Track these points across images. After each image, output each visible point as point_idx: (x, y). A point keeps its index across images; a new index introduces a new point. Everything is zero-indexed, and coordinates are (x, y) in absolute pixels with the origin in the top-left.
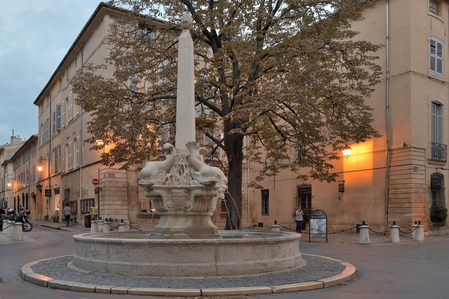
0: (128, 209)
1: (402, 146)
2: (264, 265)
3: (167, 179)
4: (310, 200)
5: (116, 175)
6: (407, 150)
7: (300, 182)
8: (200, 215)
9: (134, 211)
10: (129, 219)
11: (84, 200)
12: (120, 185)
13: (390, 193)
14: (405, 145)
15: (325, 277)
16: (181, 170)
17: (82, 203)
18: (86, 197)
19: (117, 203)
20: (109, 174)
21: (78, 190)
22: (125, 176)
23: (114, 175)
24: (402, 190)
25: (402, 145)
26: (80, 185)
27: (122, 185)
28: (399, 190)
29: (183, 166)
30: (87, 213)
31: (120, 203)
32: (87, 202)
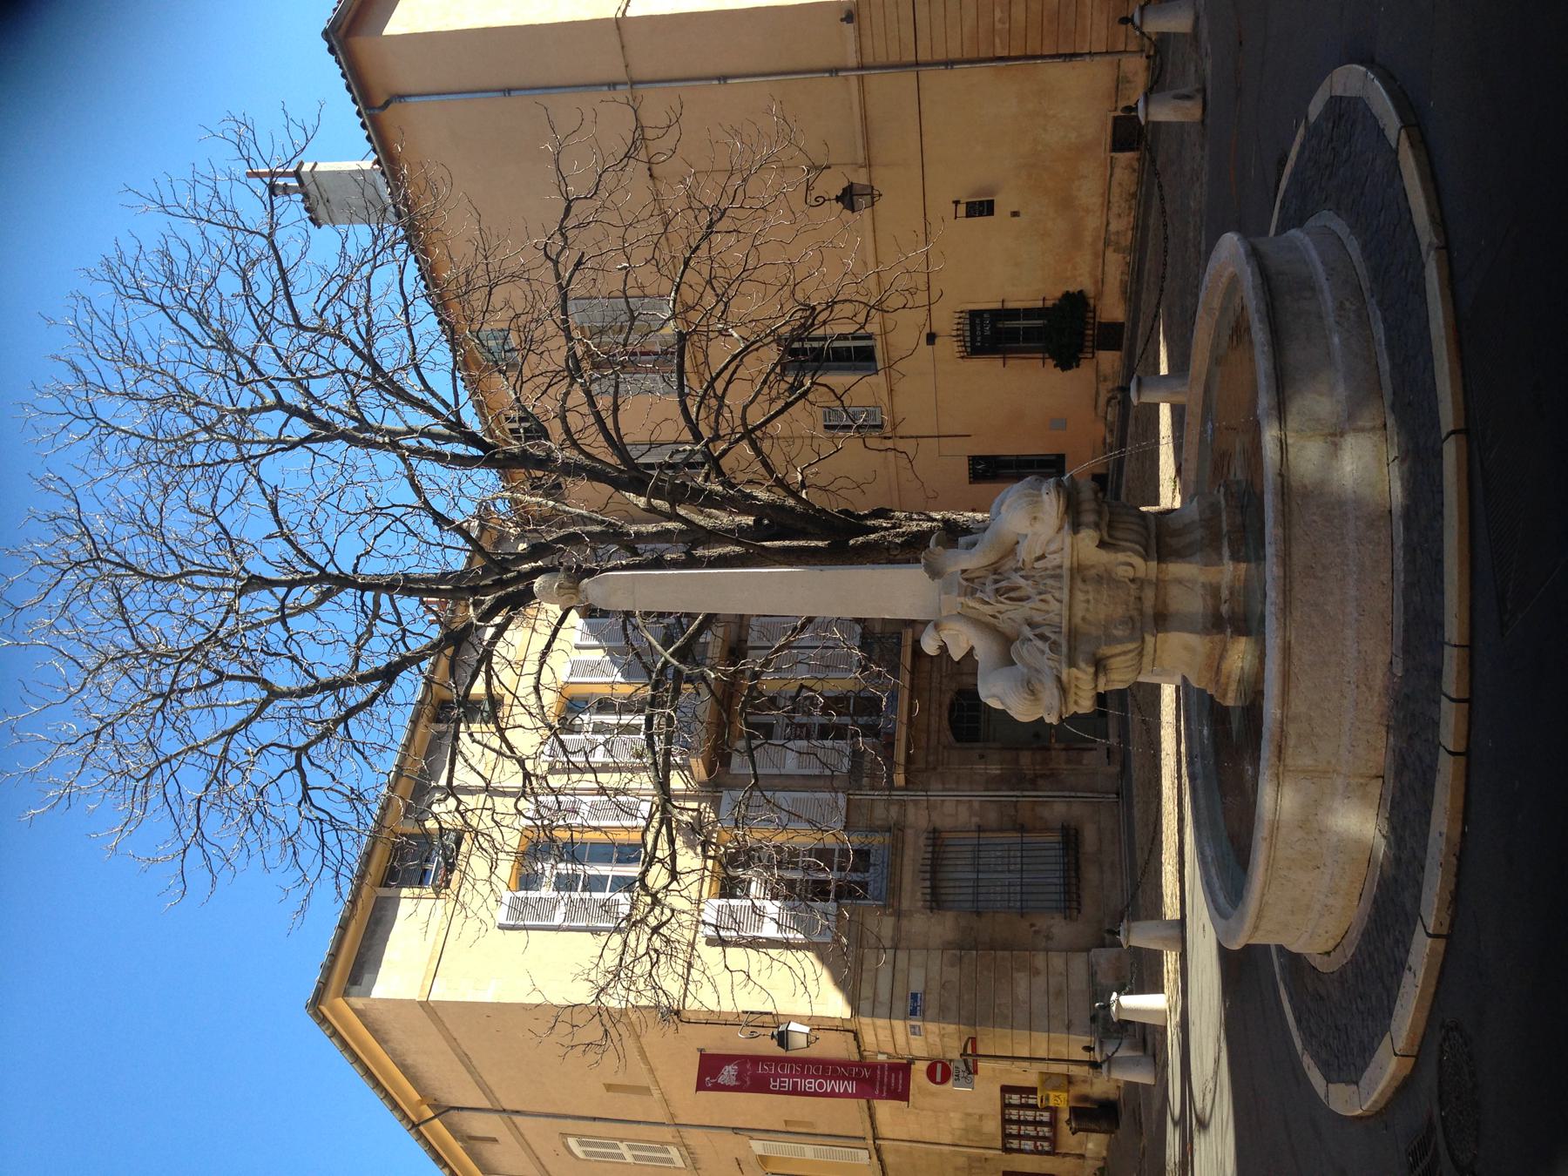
0: (1047, 950)
1: (851, 26)
2: (1341, 307)
3: (1042, 637)
4: (1014, 314)
5: (917, 986)
6: (864, 12)
7: (948, 347)
8: (1158, 537)
9: (1054, 930)
10: (1088, 950)
11: (1006, 1136)
12: (953, 974)
13: (1005, 53)
14: (849, 18)
15: (1381, 133)
16: (1012, 595)
17: (1015, 1144)
18: (993, 1126)
19: (1022, 990)
20: (913, 1013)
21: (961, 1161)
22: (918, 957)
23: (914, 996)
24: (998, 14)
25: (849, 29)
26: (941, 1154)
27: (952, 965)
28: (998, 26)
29: (997, 590)
30: (1053, 1124)
31: (1022, 979)
32: (1011, 1122)
